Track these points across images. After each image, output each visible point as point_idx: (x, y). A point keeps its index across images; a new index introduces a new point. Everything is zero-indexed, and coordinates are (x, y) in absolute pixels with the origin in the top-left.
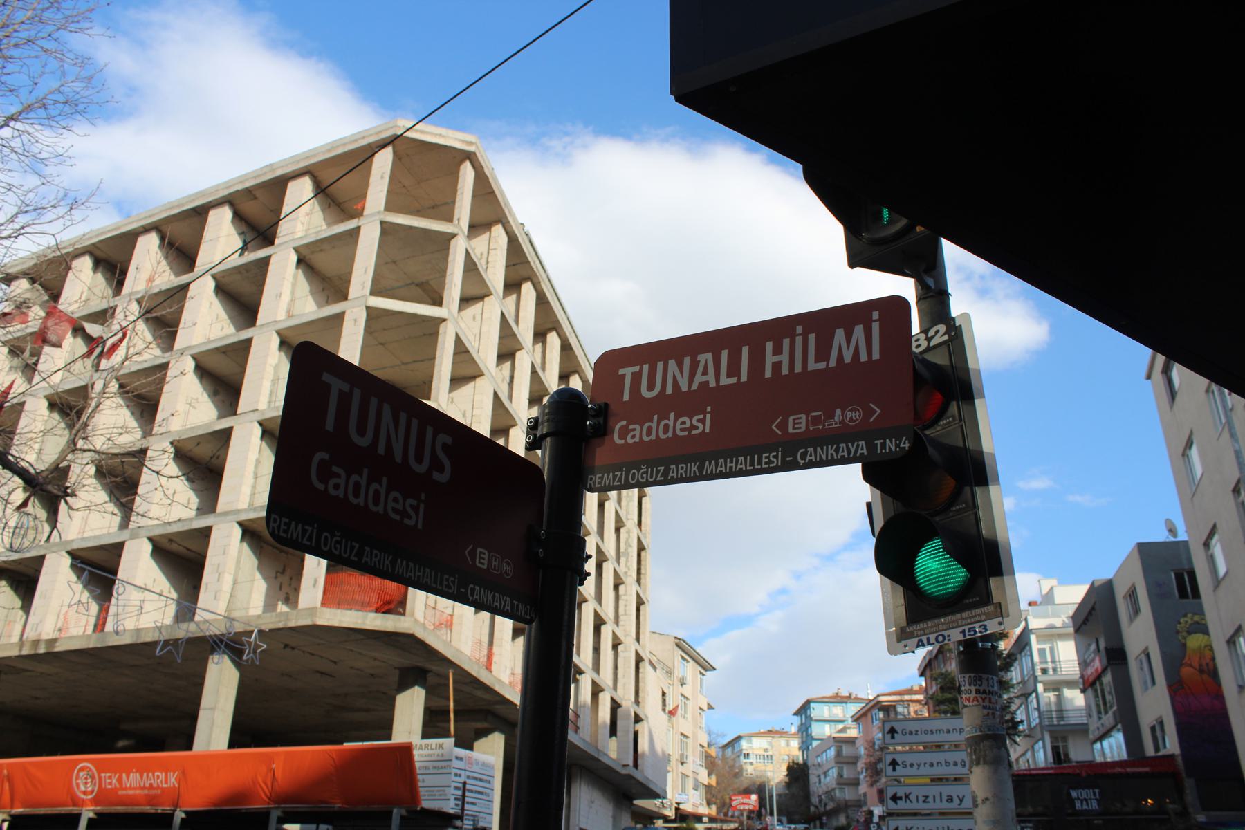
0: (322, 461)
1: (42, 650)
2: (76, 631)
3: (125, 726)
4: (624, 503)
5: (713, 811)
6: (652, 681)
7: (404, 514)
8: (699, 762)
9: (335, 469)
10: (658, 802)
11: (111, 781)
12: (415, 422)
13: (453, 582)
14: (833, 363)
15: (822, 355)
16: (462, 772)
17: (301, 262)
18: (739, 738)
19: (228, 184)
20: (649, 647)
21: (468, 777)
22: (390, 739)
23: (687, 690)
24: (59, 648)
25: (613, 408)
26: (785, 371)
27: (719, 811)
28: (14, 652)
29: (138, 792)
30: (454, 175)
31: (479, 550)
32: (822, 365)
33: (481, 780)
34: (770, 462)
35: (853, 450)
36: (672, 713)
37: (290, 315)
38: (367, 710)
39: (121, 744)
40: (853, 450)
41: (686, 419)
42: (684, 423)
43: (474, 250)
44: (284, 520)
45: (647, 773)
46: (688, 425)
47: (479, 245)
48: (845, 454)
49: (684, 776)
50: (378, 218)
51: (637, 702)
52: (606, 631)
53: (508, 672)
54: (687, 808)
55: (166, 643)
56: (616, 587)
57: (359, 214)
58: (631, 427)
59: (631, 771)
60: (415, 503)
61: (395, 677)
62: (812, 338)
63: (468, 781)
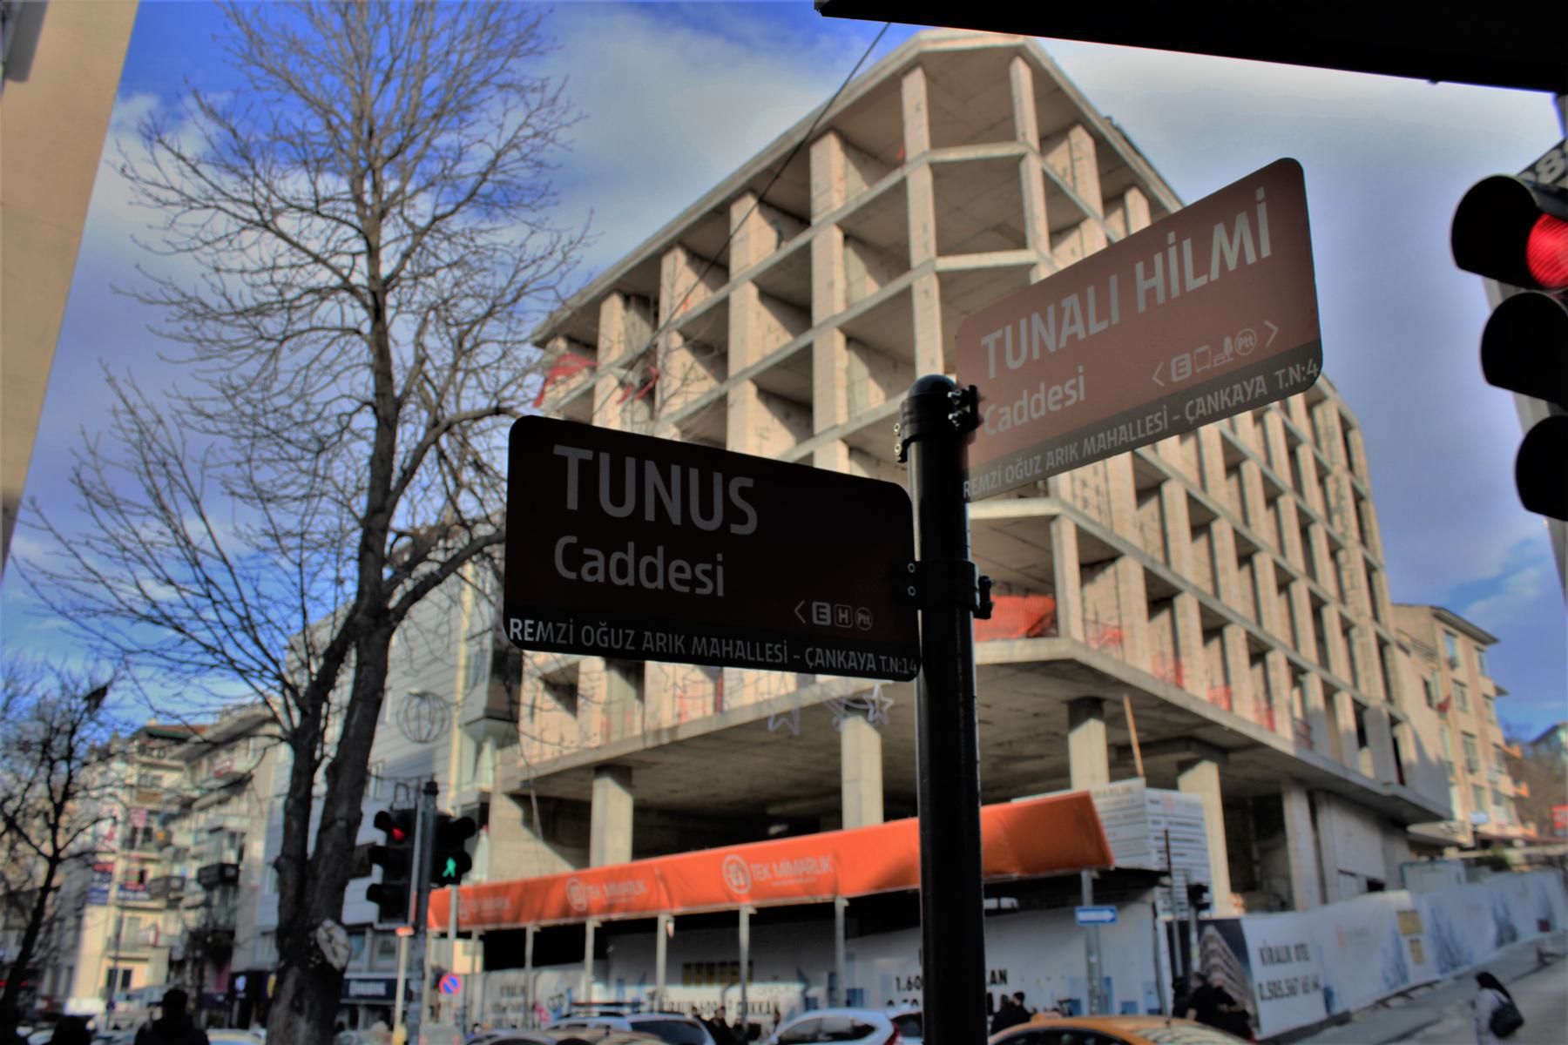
0: (567, 547)
1: (665, 740)
2: (695, 714)
3: (773, 811)
4: (1324, 444)
5: (1531, 830)
6: (1406, 668)
7: (695, 582)
8: (1495, 767)
9: (587, 551)
10: (1442, 825)
11: (762, 872)
12: (694, 474)
13: (781, 650)
14: (1215, 274)
15: (1202, 266)
16: (1162, 819)
17: (847, 238)
18: (1554, 730)
19: (744, 170)
20: (1395, 623)
21: (1171, 823)
22: (1068, 786)
23: (1461, 674)
24: (683, 735)
25: (981, 391)
26: (1161, 299)
27: (1540, 830)
28: (639, 746)
29: (792, 882)
30: (1004, 80)
31: (815, 604)
32: (1203, 280)
33: (1188, 825)
34: (1156, 426)
35: (1249, 390)
36: (1442, 708)
37: (849, 304)
38: (1041, 757)
39: (774, 830)
40: (1249, 390)
41: (1057, 388)
42: (1055, 393)
43: (1052, 167)
44: (528, 622)
45: (1418, 791)
46: (1060, 396)
47: (1059, 159)
48: (1241, 398)
49: (1477, 789)
50: (925, 161)
51: (1389, 698)
52: (1331, 615)
53: (1206, 685)
54: (1490, 829)
55: (778, 717)
56: (1333, 555)
57: (899, 163)
58: (1001, 411)
59: (1396, 789)
60: (709, 567)
61: (1063, 713)
62: (1187, 244)
63: (1171, 828)
